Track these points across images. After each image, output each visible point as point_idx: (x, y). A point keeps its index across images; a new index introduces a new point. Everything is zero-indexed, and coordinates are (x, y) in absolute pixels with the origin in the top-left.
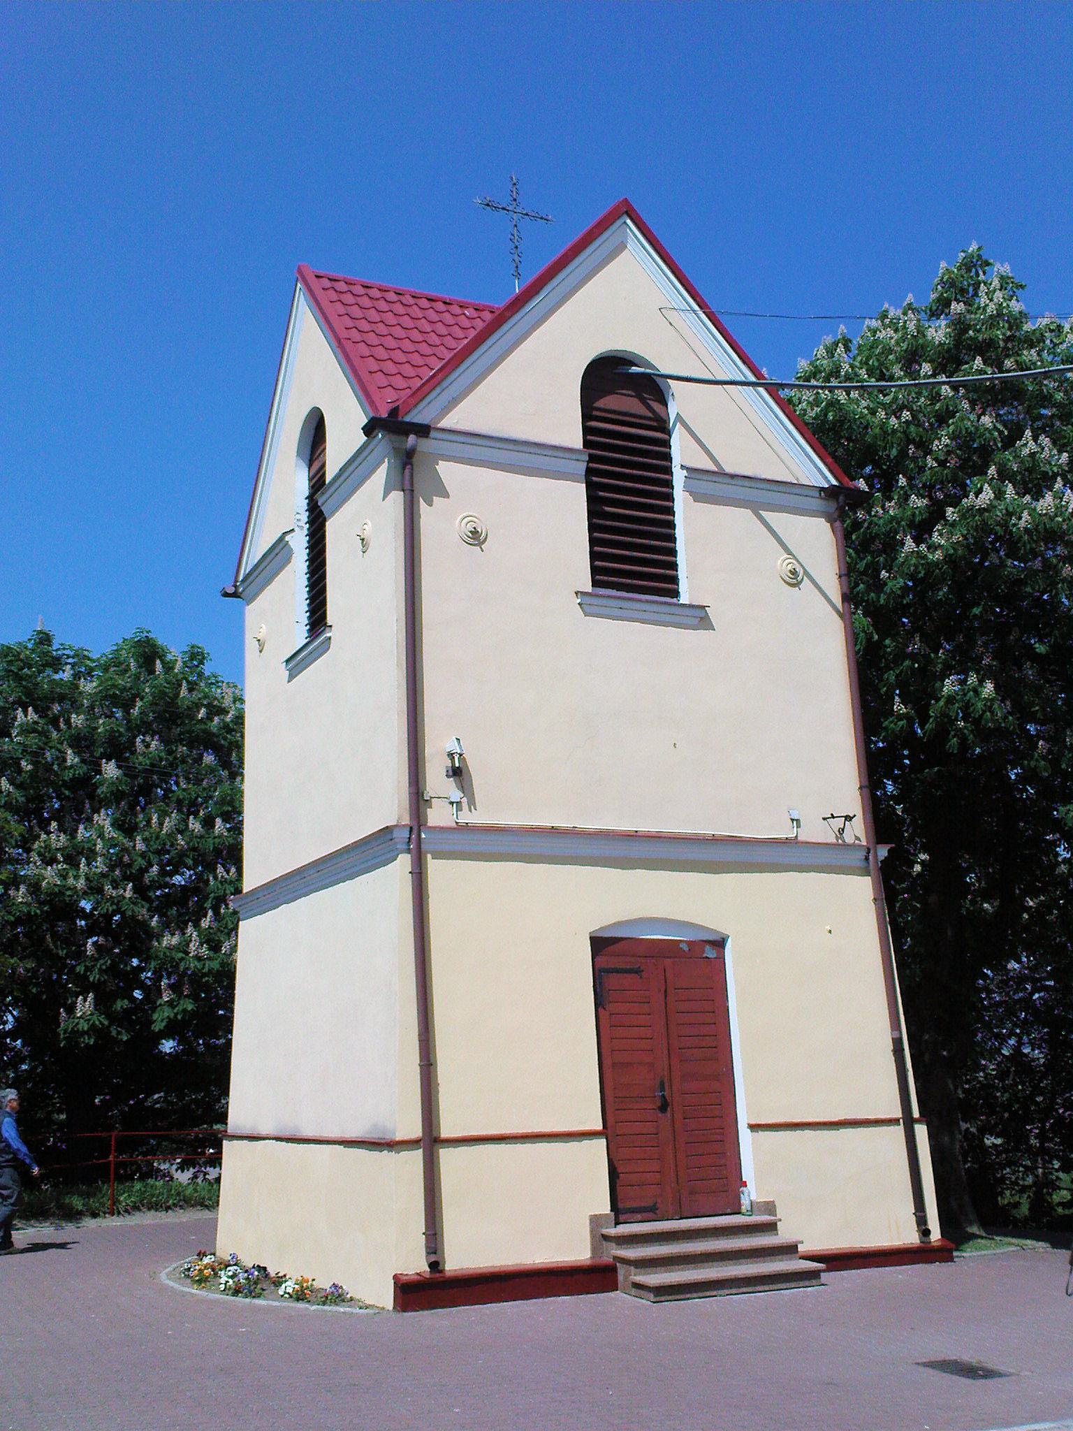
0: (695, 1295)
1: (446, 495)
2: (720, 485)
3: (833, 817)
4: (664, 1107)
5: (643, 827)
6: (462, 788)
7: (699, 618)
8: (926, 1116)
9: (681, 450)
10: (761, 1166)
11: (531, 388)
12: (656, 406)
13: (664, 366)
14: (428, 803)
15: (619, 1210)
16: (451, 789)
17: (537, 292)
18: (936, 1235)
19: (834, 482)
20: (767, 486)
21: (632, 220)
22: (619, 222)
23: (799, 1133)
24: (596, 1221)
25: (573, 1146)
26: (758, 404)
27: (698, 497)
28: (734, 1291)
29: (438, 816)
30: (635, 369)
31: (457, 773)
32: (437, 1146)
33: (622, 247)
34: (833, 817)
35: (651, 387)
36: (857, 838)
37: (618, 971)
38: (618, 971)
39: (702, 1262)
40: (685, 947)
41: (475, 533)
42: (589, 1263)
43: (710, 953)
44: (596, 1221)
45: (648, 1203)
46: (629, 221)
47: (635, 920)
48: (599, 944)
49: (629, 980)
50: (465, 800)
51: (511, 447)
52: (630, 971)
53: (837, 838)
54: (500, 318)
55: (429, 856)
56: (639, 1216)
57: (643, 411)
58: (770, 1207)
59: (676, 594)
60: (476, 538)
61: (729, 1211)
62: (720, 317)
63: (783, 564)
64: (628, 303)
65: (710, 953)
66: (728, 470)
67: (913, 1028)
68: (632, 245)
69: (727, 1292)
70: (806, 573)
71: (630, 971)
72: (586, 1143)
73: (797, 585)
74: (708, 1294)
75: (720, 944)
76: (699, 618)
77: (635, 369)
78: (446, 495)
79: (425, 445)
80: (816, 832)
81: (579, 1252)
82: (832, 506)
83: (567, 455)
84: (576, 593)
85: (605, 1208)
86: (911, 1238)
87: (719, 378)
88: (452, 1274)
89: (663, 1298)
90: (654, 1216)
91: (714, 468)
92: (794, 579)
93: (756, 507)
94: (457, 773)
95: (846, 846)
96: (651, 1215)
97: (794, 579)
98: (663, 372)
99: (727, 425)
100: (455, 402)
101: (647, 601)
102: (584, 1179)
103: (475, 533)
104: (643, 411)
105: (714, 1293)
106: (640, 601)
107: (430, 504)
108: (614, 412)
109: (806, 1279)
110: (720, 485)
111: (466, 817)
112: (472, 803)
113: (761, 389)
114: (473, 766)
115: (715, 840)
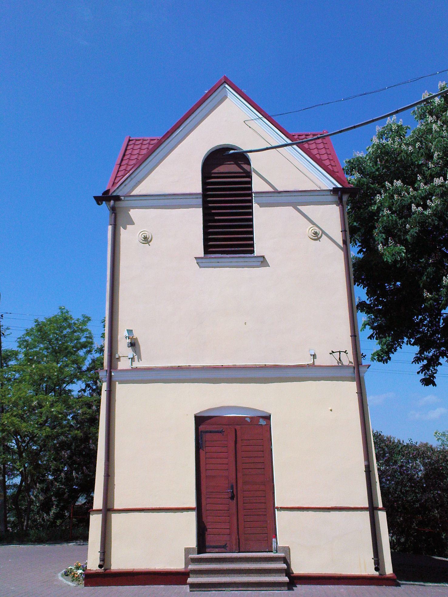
0: (212, 589)
1: (133, 223)
2: (278, 197)
3: (333, 352)
4: (232, 498)
5: (226, 363)
6: (135, 351)
7: (263, 262)
8: (386, 507)
9: (257, 185)
10: (288, 530)
11: (180, 169)
12: (245, 166)
13: (245, 149)
14: (118, 359)
15: (202, 547)
16: (130, 353)
17: (178, 127)
18: (389, 570)
19: (339, 186)
20: (300, 194)
21: (228, 85)
22: (222, 86)
23: (305, 513)
24: (188, 551)
25: (178, 514)
26: (295, 154)
27: (261, 205)
28: (235, 589)
29: (123, 364)
30: (232, 151)
31: (133, 344)
32: (108, 512)
33: (225, 97)
34: (333, 352)
35: (241, 158)
36: (350, 362)
37: (211, 432)
38: (211, 432)
39: (228, 573)
40: (249, 420)
41: (145, 238)
42: (183, 570)
43: (262, 422)
44: (188, 551)
45: (222, 544)
46: (227, 86)
47: (226, 407)
48: (200, 420)
49: (216, 436)
50: (136, 357)
51: (164, 198)
52: (218, 432)
53: (338, 363)
54: (160, 143)
55: (117, 383)
56: (217, 550)
57: (238, 169)
58: (287, 550)
59: (252, 252)
60: (146, 240)
61: (267, 550)
62: (273, 118)
63: (309, 229)
64: (231, 122)
65: (262, 422)
66: (280, 189)
67: (92, 446)
68: (230, 96)
69: (231, 589)
70: (323, 232)
71: (218, 432)
72: (185, 513)
73: (318, 239)
74: (220, 589)
75: (268, 418)
76: (263, 262)
77: (232, 151)
78: (133, 223)
79: (119, 204)
80: (325, 359)
81: (179, 565)
82: (335, 198)
83: (191, 197)
84: (196, 258)
85: (193, 543)
86: (370, 571)
87: (273, 145)
88: (114, 571)
89: (194, 590)
90: (225, 551)
91: (272, 190)
92: (316, 237)
93: (295, 205)
94: (133, 344)
95: (343, 366)
96: (223, 550)
97: (316, 237)
98: (245, 150)
99: (280, 167)
100: (140, 182)
101: (215, 258)
102: (184, 531)
103: (145, 238)
104: (238, 169)
105: (224, 589)
106: (212, 258)
107: (125, 228)
108: (223, 173)
109: (278, 586)
110: (278, 197)
111: (136, 364)
112: (140, 358)
113: (295, 146)
114: (141, 342)
115: (265, 367)
